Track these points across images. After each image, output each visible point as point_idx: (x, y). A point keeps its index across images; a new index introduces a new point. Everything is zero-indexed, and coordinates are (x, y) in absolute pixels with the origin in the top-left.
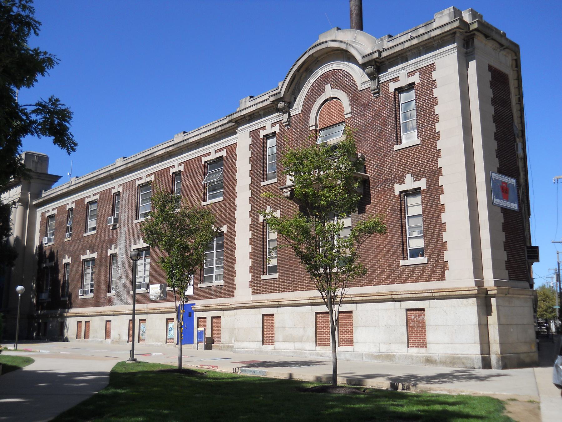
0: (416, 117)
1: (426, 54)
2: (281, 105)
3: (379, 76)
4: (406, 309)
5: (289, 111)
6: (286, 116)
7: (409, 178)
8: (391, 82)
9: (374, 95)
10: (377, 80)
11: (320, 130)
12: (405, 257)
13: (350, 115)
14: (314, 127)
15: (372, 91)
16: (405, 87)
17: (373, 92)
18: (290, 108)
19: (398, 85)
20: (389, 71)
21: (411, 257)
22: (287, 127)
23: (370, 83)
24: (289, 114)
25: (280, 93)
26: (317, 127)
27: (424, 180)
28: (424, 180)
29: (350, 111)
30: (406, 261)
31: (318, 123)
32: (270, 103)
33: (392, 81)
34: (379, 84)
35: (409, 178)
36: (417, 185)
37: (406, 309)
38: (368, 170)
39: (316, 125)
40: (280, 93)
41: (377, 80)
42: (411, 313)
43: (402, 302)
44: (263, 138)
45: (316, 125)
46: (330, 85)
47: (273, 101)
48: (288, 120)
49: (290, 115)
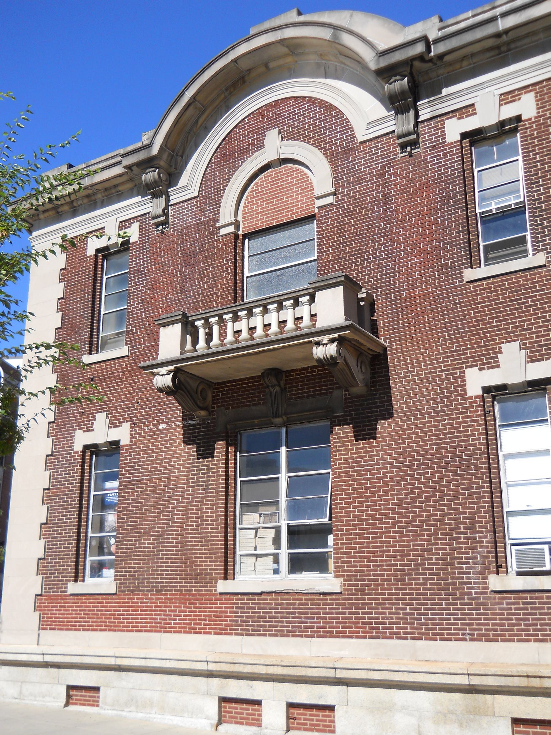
0: (316, 254)
1: (88, 212)
2: (150, 176)
3: (169, 190)
4: (511, 718)
5: (168, 193)
6: (162, 201)
7: (101, 420)
8: (525, 93)
9: (157, 227)
10: (164, 197)
11: (245, 236)
12: (501, 567)
13: (331, 200)
14: (232, 229)
15: (154, 218)
16: (490, 127)
17: (401, 141)
18: (170, 186)
19: (102, 243)
20: (445, 91)
21: (92, 576)
22: (160, 228)
23: (151, 204)
24: (168, 200)
25: (149, 146)
26: (237, 227)
27: (126, 426)
28: (126, 426)
29: (333, 190)
30: (229, 582)
31: (240, 218)
32: (124, 170)
33: (531, 91)
34: (167, 206)
35: (101, 420)
36: (114, 435)
37: (511, 718)
38: (381, 333)
39: (236, 224)
40: (149, 146)
41: (164, 197)
42: (241, 709)
43: (352, 690)
44: (96, 256)
45: (236, 224)
46: (279, 130)
47: (129, 167)
48: (165, 213)
49: (169, 201)
